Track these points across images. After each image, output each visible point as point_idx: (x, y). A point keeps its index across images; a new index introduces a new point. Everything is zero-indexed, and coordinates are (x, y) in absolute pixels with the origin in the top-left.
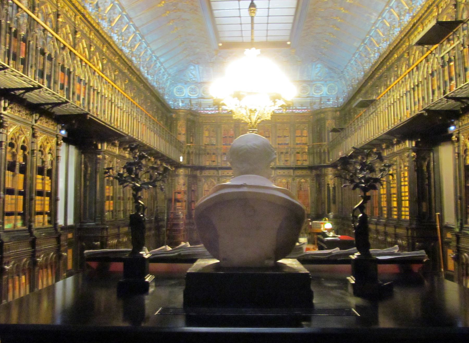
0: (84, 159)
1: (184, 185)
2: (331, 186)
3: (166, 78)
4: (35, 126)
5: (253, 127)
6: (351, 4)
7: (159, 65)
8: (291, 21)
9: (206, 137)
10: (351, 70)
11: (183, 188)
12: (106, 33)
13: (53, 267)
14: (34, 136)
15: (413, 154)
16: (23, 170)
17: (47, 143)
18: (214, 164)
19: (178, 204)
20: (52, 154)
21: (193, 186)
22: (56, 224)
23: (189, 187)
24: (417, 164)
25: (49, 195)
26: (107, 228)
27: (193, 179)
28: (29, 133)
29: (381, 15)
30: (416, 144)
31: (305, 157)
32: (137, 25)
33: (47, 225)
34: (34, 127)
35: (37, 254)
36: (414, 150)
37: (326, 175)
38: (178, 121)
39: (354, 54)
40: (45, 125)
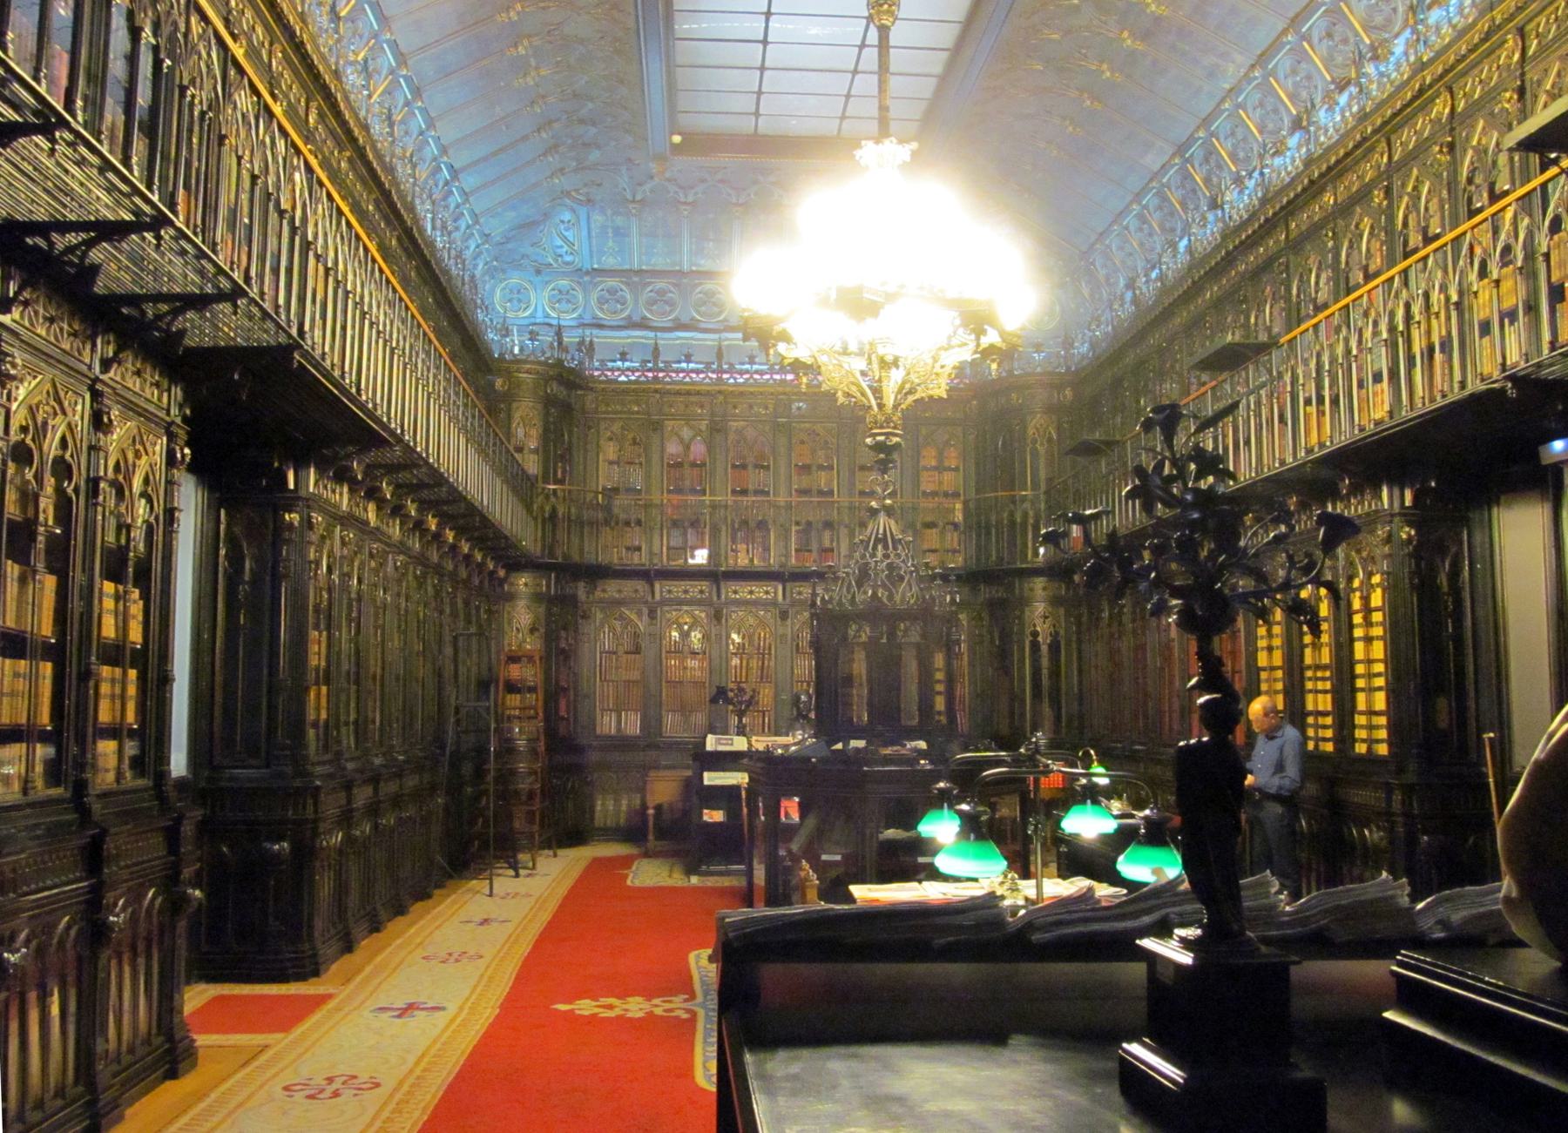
0: (229, 526)
1: (533, 630)
2: (1044, 640)
3: (473, 247)
4: (102, 381)
5: (888, 420)
6: (1158, 19)
7: (457, 197)
8: (938, 69)
9: (606, 464)
10: (1121, 248)
11: (532, 644)
12: (323, 57)
14: (99, 422)
15: (1406, 532)
17: (137, 455)
18: (639, 560)
19: (514, 700)
20: (150, 501)
21: (563, 634)
22: (161, 775)
23: (550, 638)
24: (1418, 565)
25: (140, 659)
26: (318, 788)
27: (562, 618)
28: (80, 410)
29: (1263, 59)
30: (1416, 498)
31: (952, 539)
32: (403, 47)
34: (99, 387)
35: (109, 897)
36: (1408, 517)
37: (1024, 602)
38: (515, 405)
39: (1138, 197)
40: (134, 383)
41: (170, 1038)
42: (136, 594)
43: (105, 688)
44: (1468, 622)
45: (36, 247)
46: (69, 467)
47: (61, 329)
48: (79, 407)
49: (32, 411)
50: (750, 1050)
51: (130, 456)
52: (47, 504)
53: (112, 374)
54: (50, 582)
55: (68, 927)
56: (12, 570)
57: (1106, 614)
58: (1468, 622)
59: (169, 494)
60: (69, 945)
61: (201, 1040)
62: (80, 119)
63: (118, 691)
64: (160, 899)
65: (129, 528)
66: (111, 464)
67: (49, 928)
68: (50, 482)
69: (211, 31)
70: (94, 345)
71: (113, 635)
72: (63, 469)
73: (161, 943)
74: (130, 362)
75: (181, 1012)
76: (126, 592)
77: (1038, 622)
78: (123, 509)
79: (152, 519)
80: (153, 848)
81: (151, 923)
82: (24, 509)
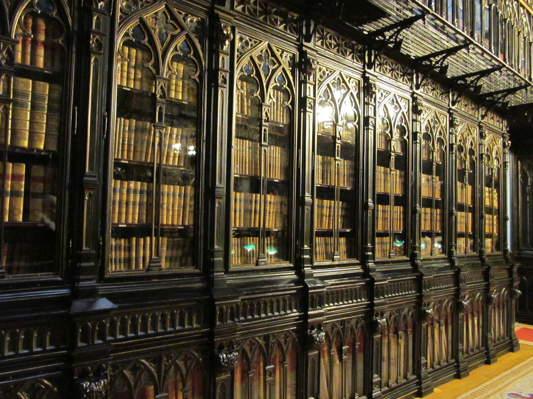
0: (521, 167)
4: (483, 123)
13: (480, 313)
14: (482, 136)
16: (441, 171)
20: (498, 160)
28: (476, 133)
33: (470, 252)
34: (481, 124)
40: (491, 122)
41: (511, 338)
42: (495, 191)
43: (487, 222)
45: (380, 40)
46: (474, 152)
47: (437, 93)
48: (475, 132)
49: (462, 135)
51: (491, 145)
52: (468, 163)
53: (456, 106)
54: (469, 188)
55: (479, 296)
56: (459, 184)
59: (504, 157)
60: (480, 302)
61: (521, 341)
62: (493, 52)
63: (491, 222)
64: (506, 292)
65: (492, 169)
66: (486, 148)
67: (474, 296)
68: (468, 156)
69: (525, 10)
70: (479, 111)
71: (488, 204)
72: (472, 152)
73: (507, 307)
74: (490, 115)
75: (514, 330)
76: (492, 190)
78: (490, 163)
79: (499, 166)
80: (504, 273)
81: (447, 311)
82: (461, 165)
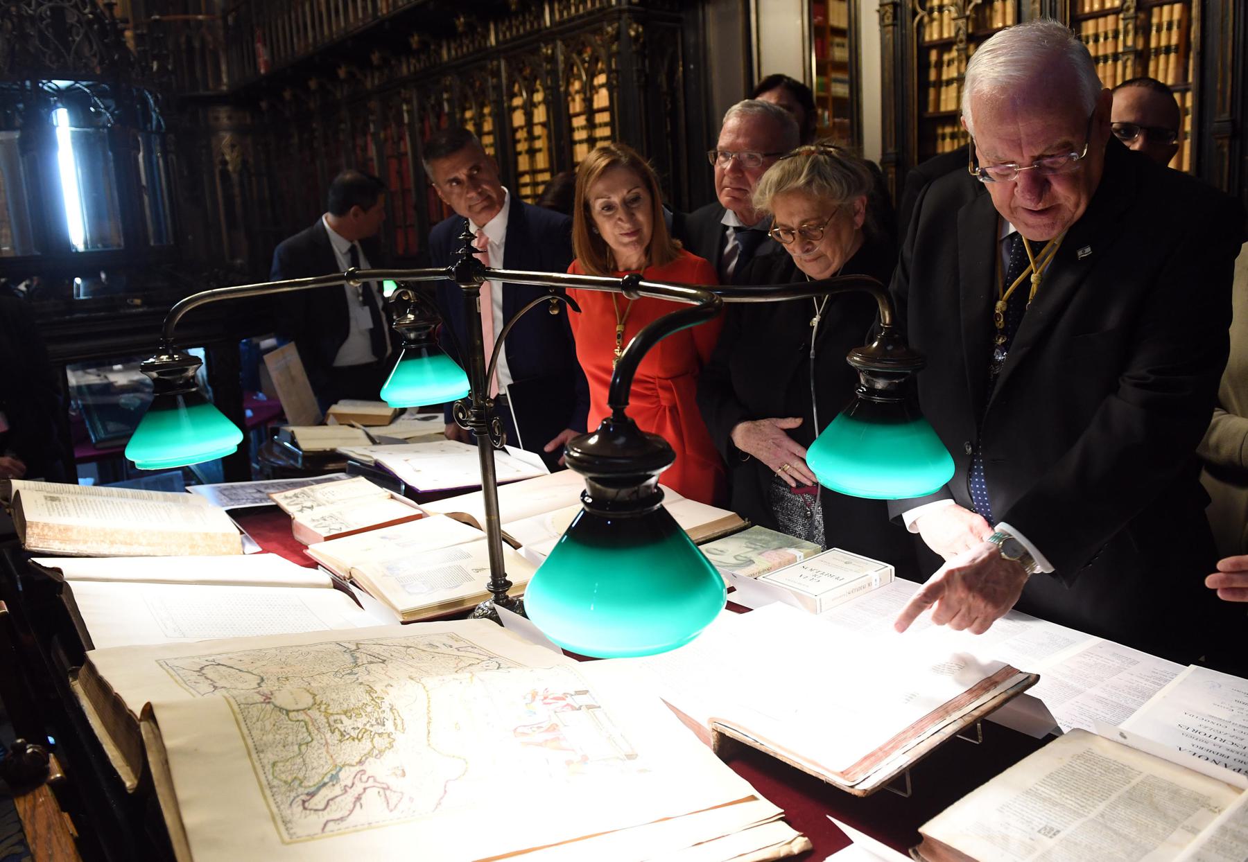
44: (682, 122)
50: (74, 370)
57: (295, 140)
58: (682, 122)
77: (227, 151)
